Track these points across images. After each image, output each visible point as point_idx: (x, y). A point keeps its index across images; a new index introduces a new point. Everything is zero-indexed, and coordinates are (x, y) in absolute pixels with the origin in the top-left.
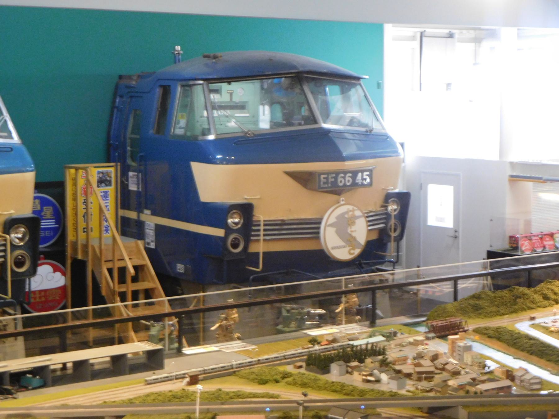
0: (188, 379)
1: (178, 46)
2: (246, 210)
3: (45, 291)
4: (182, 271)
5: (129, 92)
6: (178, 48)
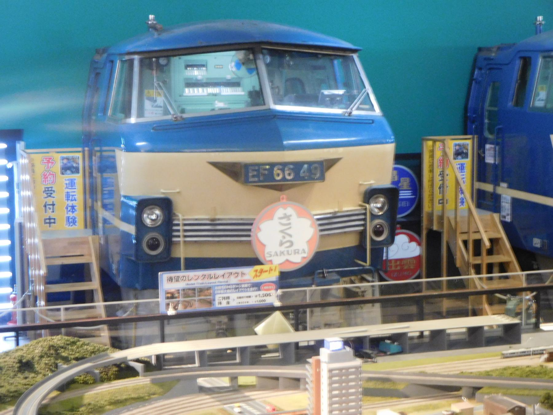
0: (546, 356)
1: (540, 15)
2: (166, 204)
3: (401, 260)
4: (538, 246)
5: (488, 64)
6: (540, 18)
